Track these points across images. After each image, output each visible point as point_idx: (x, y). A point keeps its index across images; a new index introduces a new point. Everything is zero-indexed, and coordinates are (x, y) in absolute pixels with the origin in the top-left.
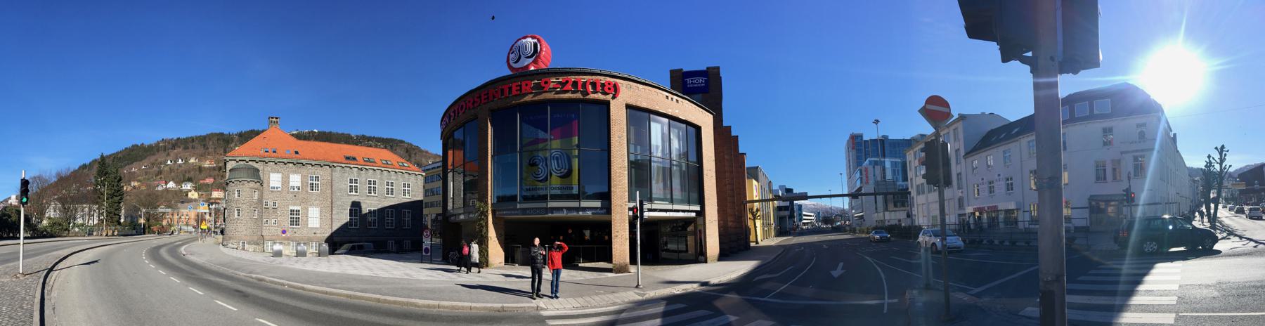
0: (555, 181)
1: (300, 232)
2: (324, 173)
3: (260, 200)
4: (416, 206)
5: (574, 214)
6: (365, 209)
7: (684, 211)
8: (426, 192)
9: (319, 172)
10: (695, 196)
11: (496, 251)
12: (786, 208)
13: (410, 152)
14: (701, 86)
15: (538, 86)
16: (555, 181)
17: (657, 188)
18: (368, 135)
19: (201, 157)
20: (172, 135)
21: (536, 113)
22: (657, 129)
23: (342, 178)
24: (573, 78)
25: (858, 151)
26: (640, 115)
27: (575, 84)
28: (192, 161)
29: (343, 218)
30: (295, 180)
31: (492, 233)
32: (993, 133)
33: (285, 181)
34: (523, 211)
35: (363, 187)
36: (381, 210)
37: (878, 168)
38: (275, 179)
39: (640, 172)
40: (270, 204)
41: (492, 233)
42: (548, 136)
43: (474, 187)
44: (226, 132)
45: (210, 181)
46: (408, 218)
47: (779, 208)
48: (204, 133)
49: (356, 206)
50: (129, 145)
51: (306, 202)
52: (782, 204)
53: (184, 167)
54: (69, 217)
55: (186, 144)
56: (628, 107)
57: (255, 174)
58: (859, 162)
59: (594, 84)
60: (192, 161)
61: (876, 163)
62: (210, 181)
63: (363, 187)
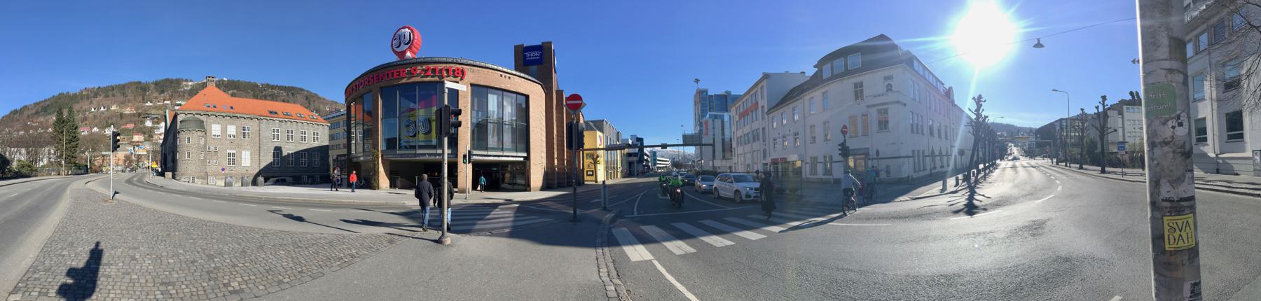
0: (421, 136)
1: (236, 170)
2: (252, 125)
3: (205, 146)
4: (323, 150)
5: (432, 158)
6: (285, 153)
7: (519, 157)
8: (332, 137)
9: (248, 123)
10: (523, 146)
11: (384, 181)
12: (635, 155)
13: (310, 100)
14: (535, 61)
15: (410, 73)
16: (421, 136)
17: (492, 140)
18: (272, 83)
19: (122, 104)
20: (94, 84)
21: (409, 90)
22: (493, 100)
23: (268, 128)
24: (432, 66)
25: (703, 105)
26: (480, 91)
27: (434, 70)
28: (114, 108)
29: (268, 159)
30: (232, 130)
31: (381, 169)
32: (792, 91)
33: (224, 130)
34: (400, 155)
35: (282, 135)
36: (297, 153)
37: (718, 122)
38: (216, 129)
39: (480, 130)
40: (213, 148)
41: (381, 169)
42: (416, 106)
43: (369, 134)
44: (143, 81)
45: (130, 126)
46: (317, 160)
47: (629, 155)
48: (123, 82)
49: (278, 150)
50: (56, 94)
51: (240, 147)
52: (631, 151)
53: (107, 114)
54: (34, 158)
55: (108, 92)
56: (472, 85)
57: (201, 126)
58: (703, 113)
59: (447, 70)
60: (114, 108)
61: (716, 117)
62: (130, 126)
63: (282, 135)
